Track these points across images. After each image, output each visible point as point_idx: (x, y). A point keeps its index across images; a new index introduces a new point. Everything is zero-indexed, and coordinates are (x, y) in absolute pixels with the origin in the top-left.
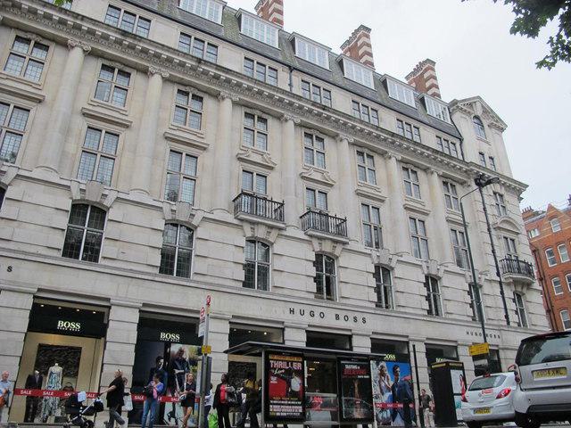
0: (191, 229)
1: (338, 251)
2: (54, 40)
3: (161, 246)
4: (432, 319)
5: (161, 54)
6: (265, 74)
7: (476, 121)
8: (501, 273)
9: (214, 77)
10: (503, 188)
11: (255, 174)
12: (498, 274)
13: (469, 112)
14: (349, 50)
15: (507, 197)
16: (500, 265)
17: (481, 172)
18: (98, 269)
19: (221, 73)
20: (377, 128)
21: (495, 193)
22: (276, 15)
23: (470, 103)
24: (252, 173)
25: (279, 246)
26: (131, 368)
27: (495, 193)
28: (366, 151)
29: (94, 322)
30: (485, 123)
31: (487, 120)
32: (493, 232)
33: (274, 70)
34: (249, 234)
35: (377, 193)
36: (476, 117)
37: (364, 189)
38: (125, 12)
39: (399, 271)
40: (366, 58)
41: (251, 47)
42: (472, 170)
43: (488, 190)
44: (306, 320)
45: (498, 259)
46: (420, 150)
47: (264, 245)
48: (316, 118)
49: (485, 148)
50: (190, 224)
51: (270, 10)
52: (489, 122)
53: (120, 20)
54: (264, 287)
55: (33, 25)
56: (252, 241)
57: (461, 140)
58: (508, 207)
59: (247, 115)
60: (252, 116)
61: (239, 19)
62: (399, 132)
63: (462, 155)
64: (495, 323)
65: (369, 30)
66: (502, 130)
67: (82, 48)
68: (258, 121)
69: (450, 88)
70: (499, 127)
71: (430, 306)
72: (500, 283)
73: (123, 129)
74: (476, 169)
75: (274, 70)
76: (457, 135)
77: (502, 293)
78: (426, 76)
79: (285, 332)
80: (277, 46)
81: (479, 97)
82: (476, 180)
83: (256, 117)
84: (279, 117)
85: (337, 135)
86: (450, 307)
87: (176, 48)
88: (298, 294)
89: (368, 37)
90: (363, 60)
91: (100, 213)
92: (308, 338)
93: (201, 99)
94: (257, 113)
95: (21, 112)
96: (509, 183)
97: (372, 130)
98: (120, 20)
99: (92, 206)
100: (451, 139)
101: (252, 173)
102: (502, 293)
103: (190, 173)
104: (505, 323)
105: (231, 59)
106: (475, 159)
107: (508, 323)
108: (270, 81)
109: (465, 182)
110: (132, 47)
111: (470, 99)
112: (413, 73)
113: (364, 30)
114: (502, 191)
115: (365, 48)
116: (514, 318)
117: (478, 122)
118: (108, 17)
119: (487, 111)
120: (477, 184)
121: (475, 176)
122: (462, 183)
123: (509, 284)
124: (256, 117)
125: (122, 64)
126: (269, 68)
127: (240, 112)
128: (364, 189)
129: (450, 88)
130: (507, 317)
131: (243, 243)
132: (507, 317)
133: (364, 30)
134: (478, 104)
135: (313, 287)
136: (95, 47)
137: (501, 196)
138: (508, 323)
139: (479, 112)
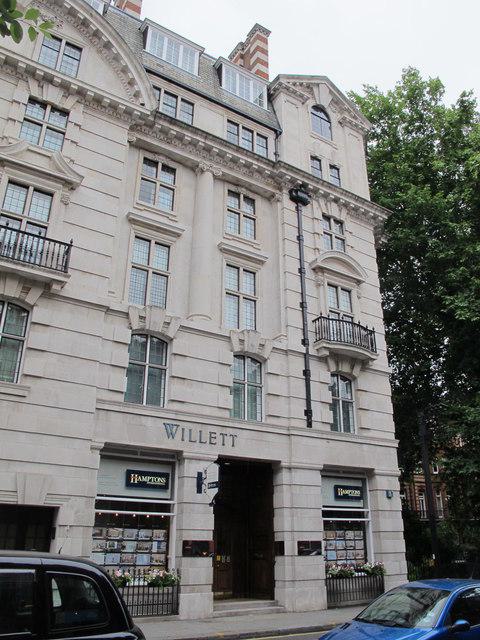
1: (32, 297)
2: (182, 162)
3: (127, 365)
5: (226, 153)
6: (176, 108)
8: (311, 338)
9: (231, 160)
11: (153, 242)
12: (305, 342)
13: (301, 96)
15: (349, 224)
16: (311, 327)
17: (300, 180)
20: (189, 127)
22: (259, 66)
23: (310, 84)
24: (238, 268)
26: (211, 533)
28: (243, 191)
30: (335, 117)
32: (309, 274)
33: (248, 130)
35: (171, 223)
36: (317, 108)
37: (144, 214)
39: (274, 364)
42: (282, 176)
43: (315, 208)
44: (215, 452)
45: (310, 318)
46: (188, 136)
47: (254, 360)
48: (190, 148)
49: (324, 151)
50: (23, 302)
51: (252, 60)
52: (339, 117)
53: (61, 54)
54: (347, 429)
55: (164, 146)
57: (278, 133)
58: (350, 240)
59: (146, 161)
60: (236, 195)
61: (145, 34)
64: (283, 422)
65: (268, 33)
67: (211, 172)
68: (163, 169)
71: (335, 420)
72: (306, 356)
73: (174, 239)
74: (290, 175)
75: (248, 130)
77: (306, 373)
80: (196, 73)
81: (325, 78)
82: (290, 192)
83: (242, 196)
84: (194, 169)
85: (273, 196)
86: (366, 419)
87: (225, 138)
88: (207, 411)
90: (253, 71)
91: (162, 343)
92: (222, 472)
93: (173, 171)
94: (243, 191)
97: (368, 209)
98: (61, 54)
99: (9, 303)
101: (150, 241)
102: (306, 373)
103: (162, 268)
104: (304, 424)
105: (210, 120)
107: (309, 425)
108: (182, 117)
109: (273, 196)
110: (180, 138)
113: (259, 33)
114: (343, 216)
115: (258, 54)
116: (322, 414)
117: (322, 115)
118: (44, 48)
120: (293, 199)
121: (290, 186)
122: (270, 198)
123: (323, 360)
124: (242, 196)
125: (167, 157)
126: (182, 100)
127: (223, 189)
128: (144, 214)
129: (281, 62)
130: (308, 413)
131: (230, 358)
132: (308, 413)
133: (259, 33)
135: (121, 381)
137: (340, 223)
138: (309, 425)
139: (325, 100)
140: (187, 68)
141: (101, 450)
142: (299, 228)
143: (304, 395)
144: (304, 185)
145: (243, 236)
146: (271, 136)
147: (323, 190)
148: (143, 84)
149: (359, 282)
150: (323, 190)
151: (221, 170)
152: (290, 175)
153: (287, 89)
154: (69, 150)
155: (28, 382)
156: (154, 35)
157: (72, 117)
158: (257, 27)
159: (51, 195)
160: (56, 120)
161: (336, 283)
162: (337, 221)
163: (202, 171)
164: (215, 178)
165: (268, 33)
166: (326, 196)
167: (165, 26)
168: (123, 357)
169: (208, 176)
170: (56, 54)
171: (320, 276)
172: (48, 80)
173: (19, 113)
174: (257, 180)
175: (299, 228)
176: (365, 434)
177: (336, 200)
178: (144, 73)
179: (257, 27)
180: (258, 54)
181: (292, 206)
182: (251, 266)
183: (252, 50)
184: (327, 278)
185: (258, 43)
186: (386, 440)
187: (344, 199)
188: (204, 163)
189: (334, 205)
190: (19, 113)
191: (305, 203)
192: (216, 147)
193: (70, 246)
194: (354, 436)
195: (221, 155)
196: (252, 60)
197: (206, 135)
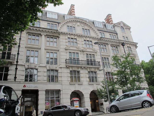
0: (57, 71)
4: (50, 83)
7: (122, 28)
10: (130, 45)
13: (119, 26)
14: (107, 20)
15: (132, 47)
17: (123, 42)
18: (8, 82)
19: (34, 28)
21: (128, 47)
23: (119, 23)
25: (98, 72)
27: (128, 47)
29: (35, 93)
31: (125, 27)
34: (89, 70)
37: (47, 48)
38: (51, 24)
40: (111, 22)
41: (111, 32)
43: (126, 46)
49: (124, 35)
56: (89, 72)
57: (117, 34)
58: (132, 50)
61: (64, 17)
62: (110, 38)
63: (118, 38)
65: (111, 15)
66: (130, 29)
69: (115, 21)
70: (129, 28)
76: (116, 33)
78: (109, 18)
79: (118, 90)
81: (122, 21)
82: (122, 44)
89: (74, 7)
90: (110, 23)
95: (28, 51)
96: (133, 44)
100: (114, 34)
104: (14, 80)
106: (122, 39)
107: (15, 80)
109: (119, 45)
111: (119, 22)
112: (106, 18)
114: (76, 37)
115: (111, 20)
117: (122, 28)
119: (124, 25)
128: (47, 48)
129: (115, 21)
134: (121, 23)
135: (69, 79)
136: (47, 34)
138: (15, 80)
139: (122, 25)
140: (102, 26)
141: (45, 91)
142: (124, 50)
143: (15, 73)
144: (124, 43)
145: (102, 52)
146: (116, 35)
147: (126, 42)
148: (98, 32)
149: (135, 57)
150: (126, 42)
151: (45, 34)
152: (121, 41)
153: (116, 25)
154: (78, 45)
155: (82, 82)
156: (66, 17)
157: (77, 39)
158: (72, 5)
159: (78, 53)
160: (75, 41)
161: (71, 52)
162: (90, 41)
163: (108, 44)
164: (45, 36)
165: (74, 5)
166: (127, 43)
167: (54, 12)
168: (69, 75)
169: (43, 36)
170: (50, 26)
171: (67, 51)
172: (86, 37)
173: (67, 41)
174: (36, 31)
175: (124, 50)
176: (39, 81)
177: (129, 44)
178: (97, 31)
179: (72, 5)
180: (73, 10)
181: (122, 46)
182: (107, 57)
183: (109, 19)
184: (68, 51)
185: (73, 8)
186: (12, 81)
187: (130, 43)
188: (108, 43)
189: (128, 44)
190: (67, 41)
191: (124, 45)
192: (47, 30)
193: (15, 55)
194: (36, 82)
195: (46, 31)
196: (110, 21)
197: (108, 38)
